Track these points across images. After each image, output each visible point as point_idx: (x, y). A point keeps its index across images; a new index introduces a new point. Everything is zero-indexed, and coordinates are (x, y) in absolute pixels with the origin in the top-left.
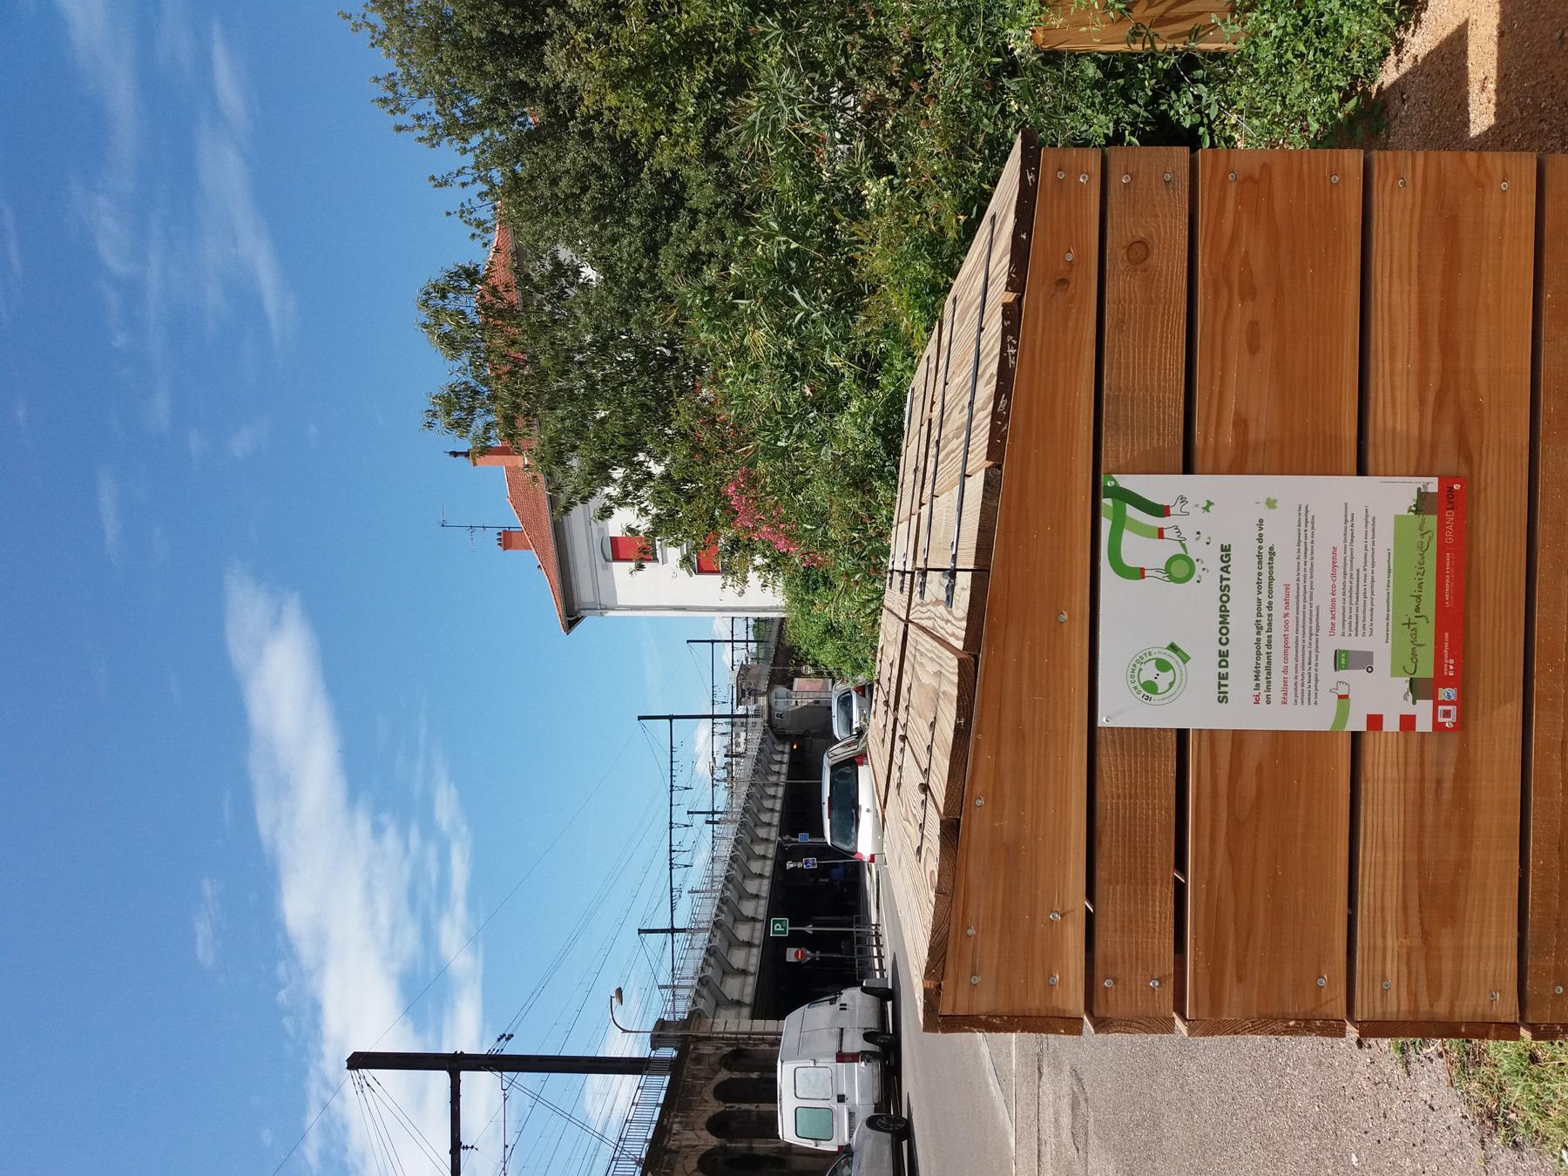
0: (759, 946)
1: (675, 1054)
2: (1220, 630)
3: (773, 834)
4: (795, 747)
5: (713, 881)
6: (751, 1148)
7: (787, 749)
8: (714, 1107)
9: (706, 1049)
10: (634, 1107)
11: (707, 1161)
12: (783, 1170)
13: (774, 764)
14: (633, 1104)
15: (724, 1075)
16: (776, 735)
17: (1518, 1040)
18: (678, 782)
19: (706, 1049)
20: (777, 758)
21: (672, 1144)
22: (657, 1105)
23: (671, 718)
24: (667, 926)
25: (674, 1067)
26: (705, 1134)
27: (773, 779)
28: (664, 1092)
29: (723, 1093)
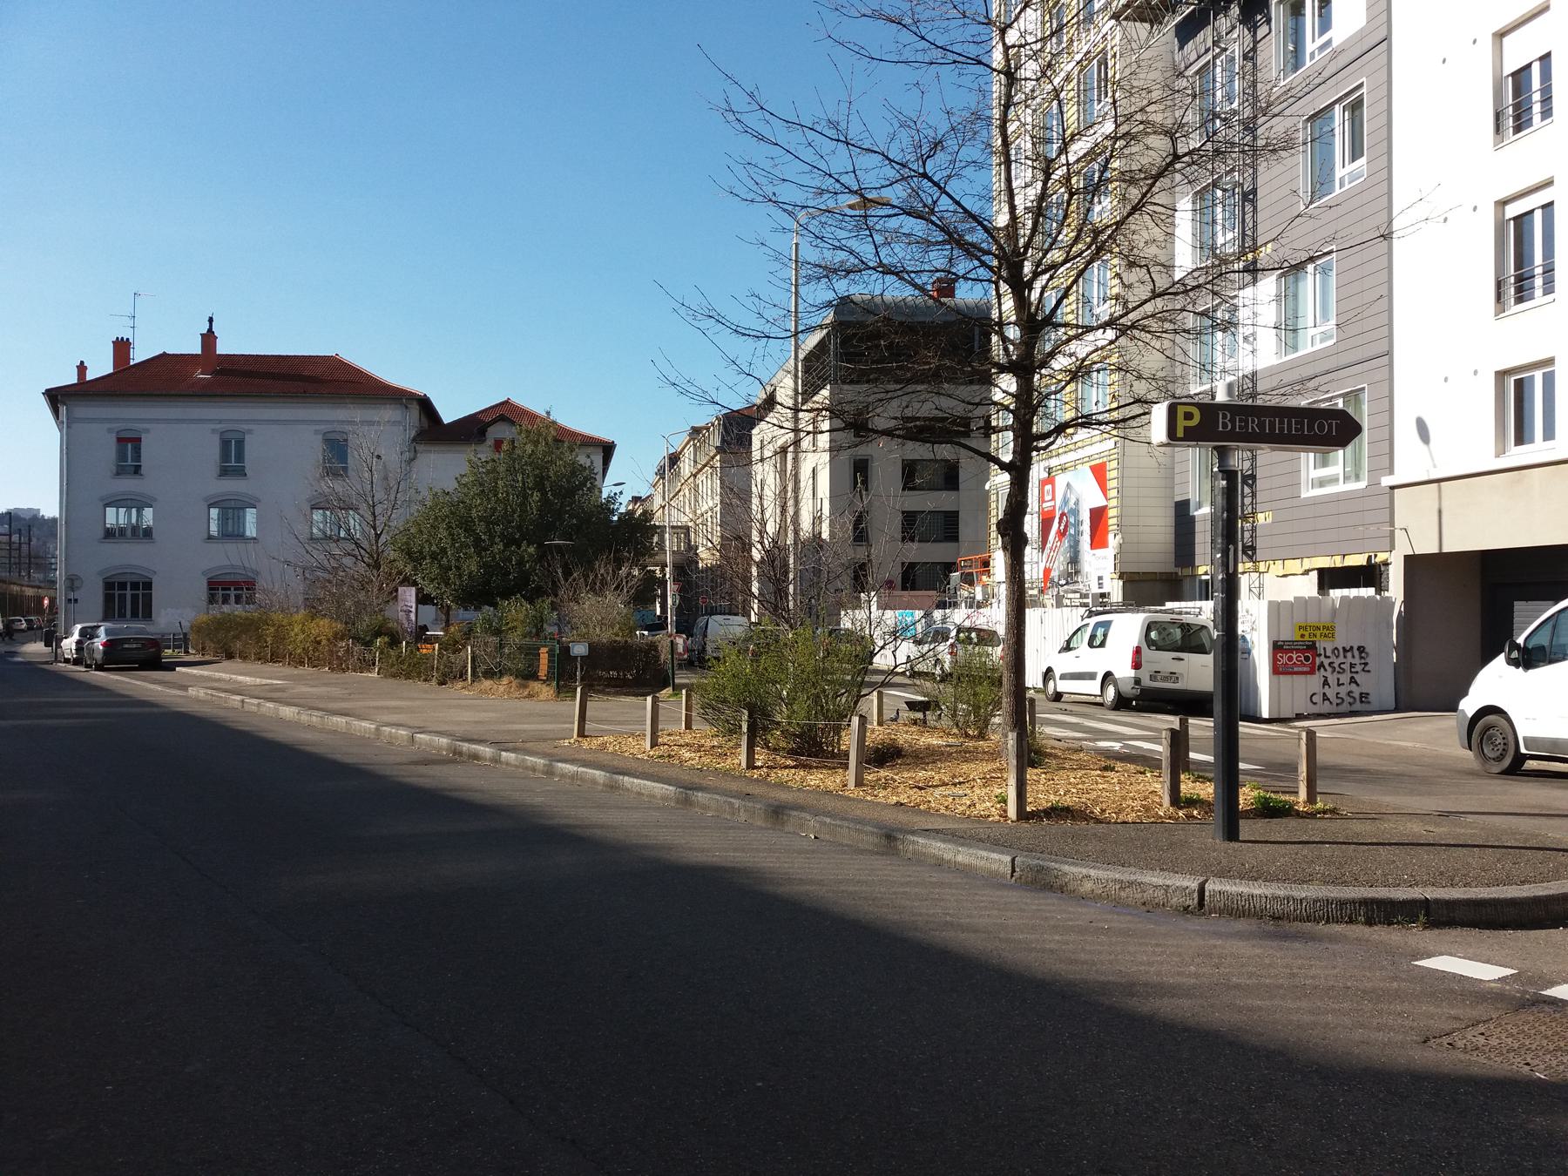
2: (1336, 648)
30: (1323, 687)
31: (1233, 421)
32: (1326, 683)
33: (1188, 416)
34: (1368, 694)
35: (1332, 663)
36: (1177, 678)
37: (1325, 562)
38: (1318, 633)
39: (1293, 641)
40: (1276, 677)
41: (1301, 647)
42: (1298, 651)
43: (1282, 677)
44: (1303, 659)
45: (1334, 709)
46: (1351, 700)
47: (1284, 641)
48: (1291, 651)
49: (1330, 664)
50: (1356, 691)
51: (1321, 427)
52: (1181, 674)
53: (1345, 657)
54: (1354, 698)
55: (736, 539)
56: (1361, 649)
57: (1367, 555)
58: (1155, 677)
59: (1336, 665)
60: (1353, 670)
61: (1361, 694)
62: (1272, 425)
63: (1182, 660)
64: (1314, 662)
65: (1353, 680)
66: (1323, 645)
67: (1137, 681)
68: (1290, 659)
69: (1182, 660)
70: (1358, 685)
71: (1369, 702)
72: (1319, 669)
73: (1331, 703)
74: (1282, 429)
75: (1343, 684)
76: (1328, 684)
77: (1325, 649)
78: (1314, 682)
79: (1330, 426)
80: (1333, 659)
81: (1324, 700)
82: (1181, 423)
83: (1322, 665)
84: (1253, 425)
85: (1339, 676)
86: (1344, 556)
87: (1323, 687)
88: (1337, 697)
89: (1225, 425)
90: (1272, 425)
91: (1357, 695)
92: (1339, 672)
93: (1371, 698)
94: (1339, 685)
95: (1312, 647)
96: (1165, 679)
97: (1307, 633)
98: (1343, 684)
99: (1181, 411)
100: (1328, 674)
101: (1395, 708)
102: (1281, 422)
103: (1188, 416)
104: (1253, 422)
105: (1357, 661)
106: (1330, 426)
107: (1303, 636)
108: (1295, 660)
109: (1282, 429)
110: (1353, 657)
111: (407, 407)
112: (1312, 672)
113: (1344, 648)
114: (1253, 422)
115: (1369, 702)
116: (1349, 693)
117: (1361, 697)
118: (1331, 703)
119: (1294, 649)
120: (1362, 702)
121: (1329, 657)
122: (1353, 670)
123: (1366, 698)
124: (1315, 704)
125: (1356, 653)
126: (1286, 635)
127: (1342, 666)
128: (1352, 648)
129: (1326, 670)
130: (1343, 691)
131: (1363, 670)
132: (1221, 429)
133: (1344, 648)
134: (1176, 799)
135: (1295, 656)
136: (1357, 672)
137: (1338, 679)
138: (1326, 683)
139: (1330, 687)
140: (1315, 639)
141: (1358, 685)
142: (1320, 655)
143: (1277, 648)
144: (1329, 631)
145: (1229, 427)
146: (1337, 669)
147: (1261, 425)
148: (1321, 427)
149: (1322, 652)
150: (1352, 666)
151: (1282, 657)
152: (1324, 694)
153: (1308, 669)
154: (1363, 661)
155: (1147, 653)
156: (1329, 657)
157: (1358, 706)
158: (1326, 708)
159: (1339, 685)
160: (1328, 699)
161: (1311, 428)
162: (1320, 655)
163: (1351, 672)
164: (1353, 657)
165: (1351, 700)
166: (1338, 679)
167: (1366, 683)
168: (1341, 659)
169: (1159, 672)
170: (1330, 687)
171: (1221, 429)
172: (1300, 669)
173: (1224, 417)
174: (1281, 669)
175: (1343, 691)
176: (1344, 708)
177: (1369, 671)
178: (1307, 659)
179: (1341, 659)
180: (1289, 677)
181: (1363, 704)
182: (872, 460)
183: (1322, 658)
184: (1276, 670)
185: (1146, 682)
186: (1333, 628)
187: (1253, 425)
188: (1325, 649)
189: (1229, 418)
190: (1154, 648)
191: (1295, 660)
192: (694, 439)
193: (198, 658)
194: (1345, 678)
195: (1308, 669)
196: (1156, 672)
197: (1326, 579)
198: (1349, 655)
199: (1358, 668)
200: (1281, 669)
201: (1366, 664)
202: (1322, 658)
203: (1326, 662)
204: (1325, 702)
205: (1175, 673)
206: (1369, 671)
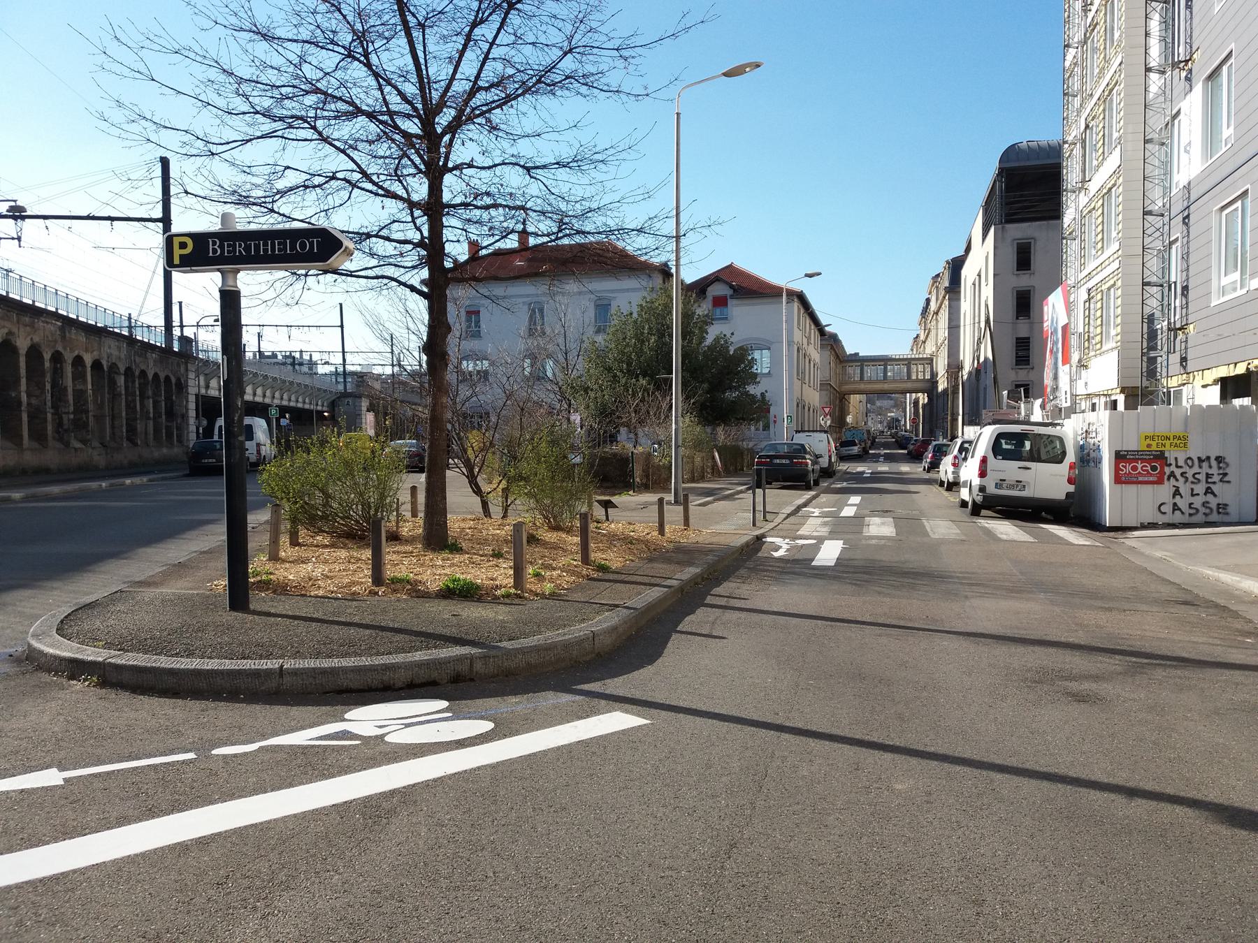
0: (206, 393)
1: (176, 349)
2: (1190, 458)
3: (277, 402)
4: (326, 414)
5: (205, 351)
6: (148, 398)
7: (325, 409)
8: (162, 376)
9: (182, 369)
10: (18, 277)
11: (7, 347)
12: (164, 417)
13: (280, 393)
14: (21, 276)
15: (173, 380)
16: (334, 401)
17: (834, 474)
18: (294, 331)
19: (182, 369)
20: (259, 391)
21: (149, 355)
22: (57, 309)
23: (342, 326)
24: (767, 510)
25: (168, 350)
26: (153, 372)
27: (293, 398)
28: (85, 321)
29: (167, 378)
30: (1174, 497)
31: (222, 247)
32: (1177, 492)
33: (183, 245)
34: (1226, 505)
35: (1186, 473)
36: (1024, 486)
37: (1224, 372)
38: (1168, 443)
39: (1138, 451)
40: (1119, 486)
41: (1147, 457)
42: (1143, 460)
43: (1131, 490)
44: (1149, 468)
45: (1186, 519)
46: (1208, 511)
47: (1127, 451)
48: (1136, 460)
49: (1182, 474)
50: (1213, 502)
51: (303, 246)
52: (1028, 483)
53: (1200, 467)
54: (1211, 509)
55: (954, 367)
56: (1219, 459)
57: (1247, 362)
58: (1001, 485)
59: (1189, 475)
60: (1210, 480)
61: (1219, 504)
62: (257, 247)
63: (1028, 468)
64: (1162, 473)
65: (1208, 491)
66: (1171, 455)
67: (982, 489)
68: (1135, 468)
69: (1028, 468)
70: (1215, 496)
71: (1227, 514)
72: (1169, 479)
73: (1183, 513)
74: (266, 251)
75: (1198, 494)
76: (1180, 494)
77: (1176, 459)
78: (1164, 491)
79: (312, 244)
80: (1186, 469)
81: (1174, 510)
82: (177, 252)
83: (1172, 475)
84: (240, 249)
85: (1193, 486)
86: (1236, 364)
87: (1174, 497)
88: (1190, 507)
89: (215, 251)
90: (257, 247)
91: (1214, 506)
92: (1192, 483)
93: (1229, 509)
94: (1193, 495)
95: (1160, 457)
96: (1011, 487)
97: (1154, 444)
98: (1198, 494)
99: (176, 241)
100: (1180, 484)
101: (1256, 521)
102: (265, 244)
103: (183, 245)
104: (240, 246)
105: (1214, 471)
106: (312, 244)
107: (1149, 446)
108: (1139, 469)
109: (266, 251)
110: (1210, 467)
111: (650, 276)
112: (1160, 481)
113: (1199, 459)
114: (240, 246)
115: (1227, 514)
116: (1205, 504)
117: (1218, 508)
118: (1183, 513)
119: (1138, 459)
120: (1219, 513)
121: (1181, 467)
122: (1210, 480)
123: (1224, 509)
124: (1165, 513)
125: (1214, 463)
126: (1132, 444)
127: (1197, 476)
128: (1208, 458)
129: (1177, 480)
130: (1198, 502)
131: (1221, 481)
132: (211, 254)
133: (1199, 459)
134: (378, 578)
135: (1139, 466)
136: (1214, 483)
137: (1192, 490)
138: (1177, 492)
139: (1182, 497)
140: (1163, 449)
141: (1215, 496)
142: (1170, 465)
143: (1119, 457)
144: (1182, 441)
145: (219, 251)
146: (1191, 479)
147: (247, 249)
148: (303, 246)
149: (1173, 462)
150: (1208, 476)
151: (1125, 467)
152: (1175, 504)
153: (1155, 479)
154: (1221, 472)
155: (994, 463)
156: (1181, 467)
157: (1214, 517)
158: (1178, 518)
159: (1193, 495)
160: (1179, 509)
161: (293, 247)
162: (1170, 465)
163: (1207, 482)
164: (1210, 467)
165: (1208, 511)
166: (1192, 490)
167: (1224, 493)
168: (1196, 469)
169: (1004, 480)
170: (1182, 497)
171: (211, 254)
172: (1146, 479)
173: (214, 243)
174: (1123, 479)
175: (1198, 502)
176: (1199, 518)
177: (1229, 482)
178: (1154, 468)
179: (1196, 469)
180: (1133, 488)
181: (1221, 515)
182: (1034, 290)
183: (1173, 468)
184: (1118, 479)
185: (991, 489)
186: (1185, 438)
187: (240, 249)
188: (1176, 459)
189: (218, 244)
190: (1001, 457)
191: (1139, 469)
192: (936, 282)
193: (52, 457)
194: (1200, 489)
195: (1155, 479)
196: (1001, 480)
197: (1229, 389)
198: (1205, 465)
199: (1216, 478)
200: (1123, 479)
201: (1225, 474)
202: (1173, 468)
203: (1178, 472)
204: (1176, 512)
205: (1021, 482)
206: (1229, 482)
